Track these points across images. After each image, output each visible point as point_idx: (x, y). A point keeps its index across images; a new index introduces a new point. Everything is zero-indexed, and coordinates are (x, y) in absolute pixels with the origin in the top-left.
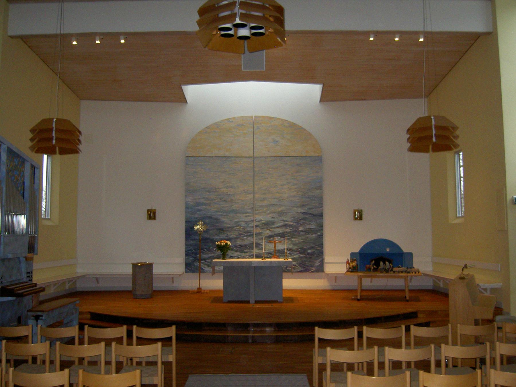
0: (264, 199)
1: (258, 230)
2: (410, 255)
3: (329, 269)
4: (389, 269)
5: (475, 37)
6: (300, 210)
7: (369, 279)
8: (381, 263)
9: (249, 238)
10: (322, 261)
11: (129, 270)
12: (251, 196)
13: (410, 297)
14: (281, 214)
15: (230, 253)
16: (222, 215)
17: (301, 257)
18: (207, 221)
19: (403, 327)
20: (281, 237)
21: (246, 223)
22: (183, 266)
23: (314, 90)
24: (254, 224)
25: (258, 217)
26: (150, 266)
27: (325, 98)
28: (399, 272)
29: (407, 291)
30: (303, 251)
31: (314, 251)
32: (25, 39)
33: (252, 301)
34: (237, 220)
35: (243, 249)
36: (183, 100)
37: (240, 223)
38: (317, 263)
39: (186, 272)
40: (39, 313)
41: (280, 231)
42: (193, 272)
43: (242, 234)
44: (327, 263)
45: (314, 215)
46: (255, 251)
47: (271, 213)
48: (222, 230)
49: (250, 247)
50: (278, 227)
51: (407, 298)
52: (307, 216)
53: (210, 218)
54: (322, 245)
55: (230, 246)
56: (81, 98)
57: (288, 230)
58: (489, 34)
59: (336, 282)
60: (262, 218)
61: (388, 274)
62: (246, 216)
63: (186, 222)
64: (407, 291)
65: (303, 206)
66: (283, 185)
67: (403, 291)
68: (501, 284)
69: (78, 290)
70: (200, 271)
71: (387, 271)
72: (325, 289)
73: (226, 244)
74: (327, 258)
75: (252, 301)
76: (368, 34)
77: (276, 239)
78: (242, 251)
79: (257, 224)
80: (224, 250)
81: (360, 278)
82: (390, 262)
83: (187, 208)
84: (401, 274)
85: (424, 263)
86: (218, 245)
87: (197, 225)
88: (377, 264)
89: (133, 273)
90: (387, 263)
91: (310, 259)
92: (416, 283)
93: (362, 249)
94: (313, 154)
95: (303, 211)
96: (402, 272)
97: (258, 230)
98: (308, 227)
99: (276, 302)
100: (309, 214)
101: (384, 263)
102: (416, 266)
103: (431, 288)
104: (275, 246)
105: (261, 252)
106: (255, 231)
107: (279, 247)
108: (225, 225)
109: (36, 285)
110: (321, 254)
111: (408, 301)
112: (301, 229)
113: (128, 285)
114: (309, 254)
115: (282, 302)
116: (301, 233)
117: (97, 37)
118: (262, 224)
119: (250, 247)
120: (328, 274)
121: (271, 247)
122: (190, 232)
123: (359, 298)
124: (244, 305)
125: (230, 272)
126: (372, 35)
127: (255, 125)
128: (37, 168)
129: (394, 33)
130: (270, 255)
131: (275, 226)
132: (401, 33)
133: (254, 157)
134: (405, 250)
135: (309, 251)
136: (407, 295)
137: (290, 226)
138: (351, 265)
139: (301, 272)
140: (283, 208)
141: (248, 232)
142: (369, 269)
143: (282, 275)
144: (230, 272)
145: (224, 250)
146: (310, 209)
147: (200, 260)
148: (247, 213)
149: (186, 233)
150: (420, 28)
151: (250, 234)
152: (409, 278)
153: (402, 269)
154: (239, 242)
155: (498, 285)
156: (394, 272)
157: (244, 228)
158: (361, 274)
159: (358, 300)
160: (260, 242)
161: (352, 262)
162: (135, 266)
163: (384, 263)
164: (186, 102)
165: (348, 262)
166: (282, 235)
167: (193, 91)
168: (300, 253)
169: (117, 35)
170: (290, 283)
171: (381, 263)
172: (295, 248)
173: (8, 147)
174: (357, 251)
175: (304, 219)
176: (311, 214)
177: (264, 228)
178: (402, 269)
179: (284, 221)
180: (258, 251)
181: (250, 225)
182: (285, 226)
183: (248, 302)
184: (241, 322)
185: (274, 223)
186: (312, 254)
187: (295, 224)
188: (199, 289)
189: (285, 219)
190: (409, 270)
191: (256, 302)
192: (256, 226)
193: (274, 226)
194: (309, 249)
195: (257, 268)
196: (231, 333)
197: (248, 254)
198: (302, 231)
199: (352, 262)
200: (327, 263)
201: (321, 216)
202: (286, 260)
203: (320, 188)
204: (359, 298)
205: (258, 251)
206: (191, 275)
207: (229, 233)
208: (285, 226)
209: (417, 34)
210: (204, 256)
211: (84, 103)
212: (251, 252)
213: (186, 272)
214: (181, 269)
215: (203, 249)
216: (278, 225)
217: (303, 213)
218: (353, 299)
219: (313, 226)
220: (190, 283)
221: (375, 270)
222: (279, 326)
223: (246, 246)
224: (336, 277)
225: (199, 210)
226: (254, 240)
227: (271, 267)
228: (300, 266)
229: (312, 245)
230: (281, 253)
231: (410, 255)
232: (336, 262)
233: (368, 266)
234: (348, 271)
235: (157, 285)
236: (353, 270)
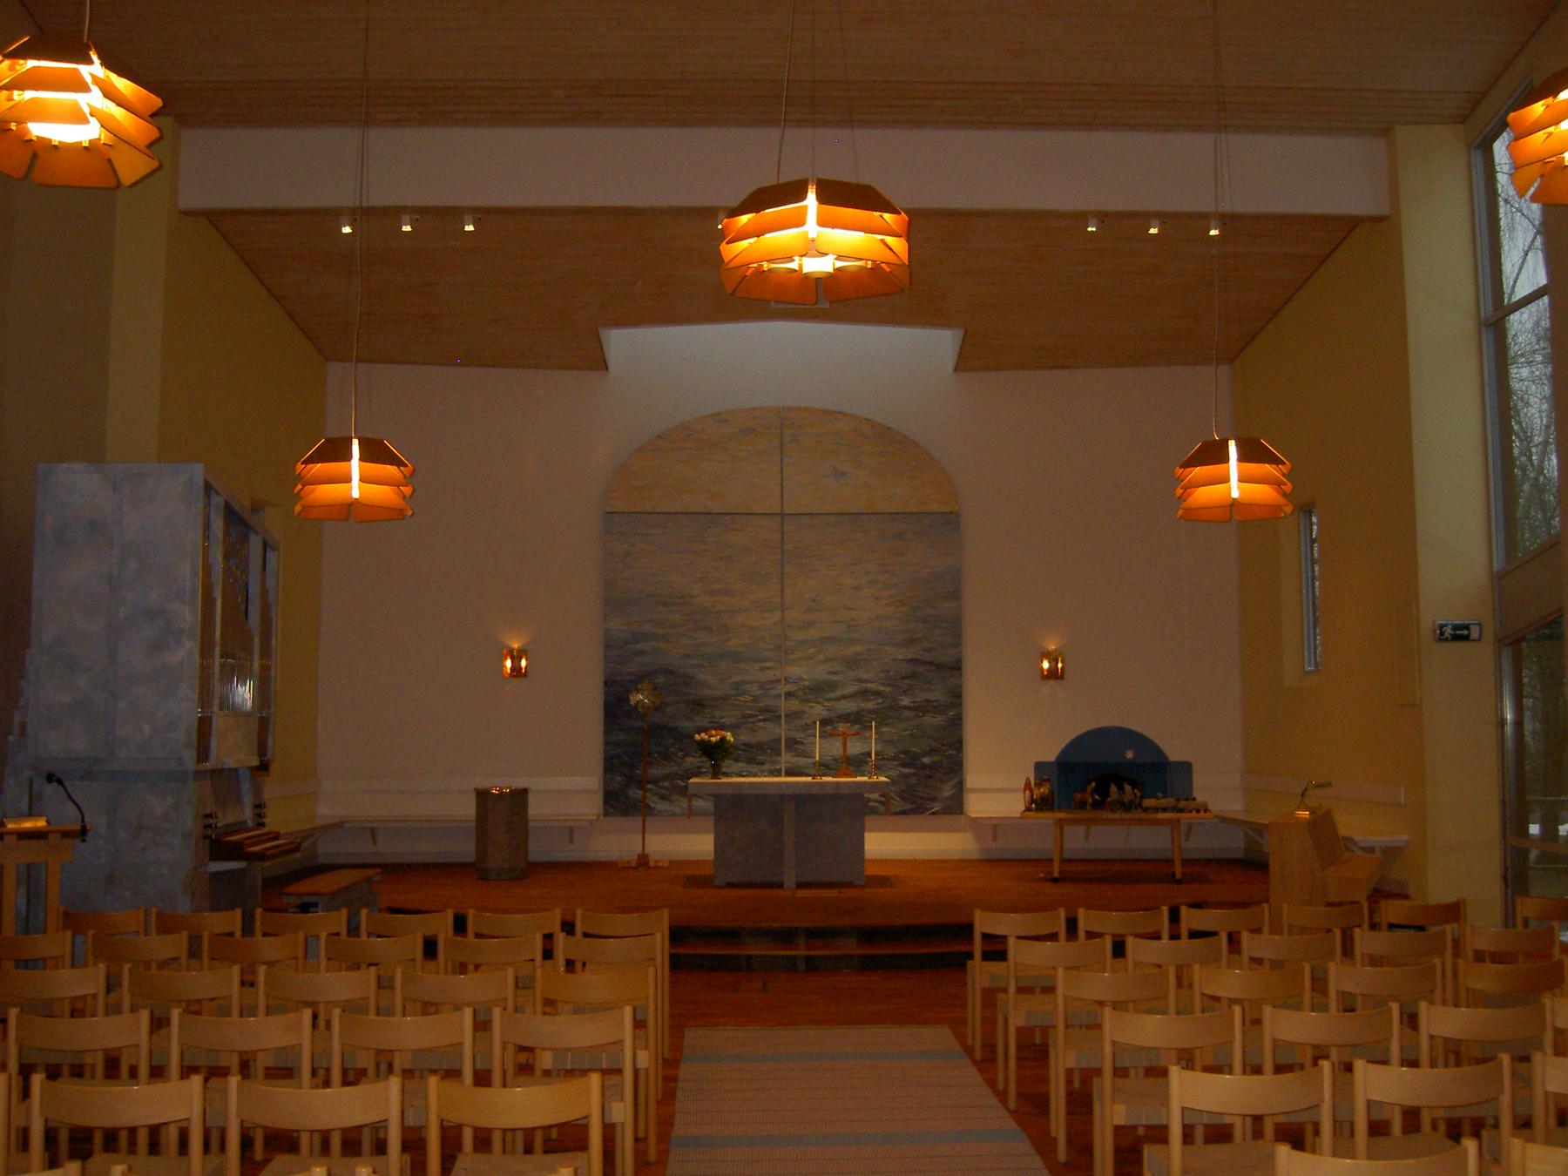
0: (810, 624)
1: (794, 705)
2: (1186, 767)
3: (978, 806)
4: (1131, 802)
5: (1343, 229)
6: (902, 654)
7: (1080, 830)
8: (1113, 789)
9: (769, 725)
10: (960, 786)
11: (467, 809)
12: (777, 616)
13: (1183, 874)
14: (852, 662)
15: (728, 764)
16: (700, 666)
17: (907, 776)
18: (661, 680)
19: (1165, 909)
20: (854, 722)
21: (762, 686)
22: (598, 799)
23: (941, 343)
24: (783, 689)
25: (794, 671)
26: (520, 795)
27: (963, 363)
28: (1157, 810)
29: (1178, 864)
30: (910, 759)
31: (936, 758)
32: (214, 217)
33: (790, 880)
34: (739, 678)
35: (755, 754)
36: (599, 363)
37: (747, 687)
38: (947, 791)
39: (606, 814)
40: (310, 899)
41: (848, 706)
42: (626, 812)
43: (751, 716)
44: (975, 790)
45: (940, 667)
46: (786, 759)
47: (827, 660)
48: (698, 705)
49: (773, 748)
50: (844, 697)
51: (1178, 876)
52: (921, 669)
53: (667, 672)
54: (958, 745)
55: (732, 746)
56: (327, 360)
57: (870, 705)
58: (1380, 219)
59: (994, 838)
60: (803, 671)
61: (1130, 816)
62: (762, 669)
63: (605, 683)
64: (1178, 864)
65: (910, 642)
66: (857, 588)
67: (1169, 862)
68: (1405, 837)
69: (321, 860)
70: (641, 810)
71: (1127, 807)
72: (966, 857)
73: (723, 739)
74: (972, 779)
75: (790, 880)
76: (1082, 217)
77: (841, 727)
78: (751, 761)
79: (790, 688)
80: (715, 754)
81: (1061, 824)
82: (1134, 785)
83: (608, 647)
84: (1161, 816)
85: (1220, 789)
86: (702, 741)
87: (638, 691)
88: (1105, 793)
89: (478, 815)
90: (1128, 788)
91: (930, 782)
92: (1200, 844)
93: (1065, 752)
94: (935, 507)
95: (910, 656)
96: (1164, 810)
97: (794, 705)
98: (924, 696)
99: (850, 885)
100: (925, 663)
101: (1121, 789)
102: (1200, 795)
103: (1240, 855)
104: (845, 745)
105: (802, 761)
106: (784, 706)
107: (855, 748)
108: (708, 692)
109: (277, 836)
110: (955, 767)
111: (1178, 882)
112: (906, 701)
113: (466, 850)
114: (924, 767)
115: (863, 887)
116: (907, 713)
117: (406, 218)
118: (805, 687)
119: (773, 748)
120: (975, 820)
121: (835, 748)
122: (616, 708)
123: (1056, 874)
124: (770, 892)
125: (733, 811)
126: (1091, 221)
127: (782, 429)
128: (273, 549)
129: (1147, 217)
130: (826, 767)
131: (839, 693)
132: (1163, 217)
133: (782, 515)
134: (1174, 755)
135: (926, 760)
136: (1178, 870)
137: (878, 693)
138: (1036, 793)
139: (904, 813)
140: (859, 648)
141: (765, 710)
142: (1082, 805)
143: (863, 823)
144: (733, 811)
145: (715, 754)
146: (929, 650)
147: (641, 783)
148: (764, 660)
149: (606, 712)
150: (1206, 206)
151: (771, 714)
152: (1183, 829)
153: (1163, 802)
154: (745, 737)
155: (1401, 838)
156: (1146, 810)
157: (756, 699)
158: (1062, 815)
159: (1055, 880)
160: (798, 735)
161: (1038, 785)
162: (482, 795)
163: (1121, 789)
164: (605, 367)
165: (1027, 786)
166: (857, 719)
167: (620, 342)
168: (904, 765)
169: (455, 214)
170: (885, 844)
171: (1113, 789)
172: (890, 752)
173: (227, 506)
174: (1051, 756)
175: (913, 675)
176: (930, 663)
177: (809, 701)
178: (1163, 802)
179: (860, 681)
180: (794, 760)
181: (774, 692)
182: (865, 694)
183: (781, 886)
184: (776, 925)
185: (832, 686)
186: (934, 767)
187: (889, 689)
188: (643, 860)
189: (865, 676)
190: (1182, 804)
191: (800, 886)
192: (789, 695)
193: (833, 695)
194: (925, 754)
195: (802, 799)
196: (758, 950)
197: (767, 767)
198: (908, 708)
199: (1038, 785)
200: (975, 790)
201: (957, 667)
202: (875, 779)
203: (956, 595)
204: (1056, 874)
205: (794, 760)
206: (619, 821)
207: (718, 713)
208: (865, 694)
209: (1204, 219)
210: (655, 772)
211: (335, 370)
212: (776, 762)
213: (606, 814)
214: (592, 806)
215: (649, 755)
216: (846, 691)
217: (910, 661)
218: (1045, 880)
219: (936, 695)
220: (618, 842)
221: (1097, 805)
222: (869, 935)
223: (761, 747)
224: (996, 827)
225: (643, 653)
226: (782, 730)
227: (835, 797)
228: (903, 799)
229: (934, 745)
230: (856, 764)
231: (1186, 767)
232: (996, 787)
233: (1079, 795)
234: (1028, 809)
235: (538, 850)
236: (1041, 804)
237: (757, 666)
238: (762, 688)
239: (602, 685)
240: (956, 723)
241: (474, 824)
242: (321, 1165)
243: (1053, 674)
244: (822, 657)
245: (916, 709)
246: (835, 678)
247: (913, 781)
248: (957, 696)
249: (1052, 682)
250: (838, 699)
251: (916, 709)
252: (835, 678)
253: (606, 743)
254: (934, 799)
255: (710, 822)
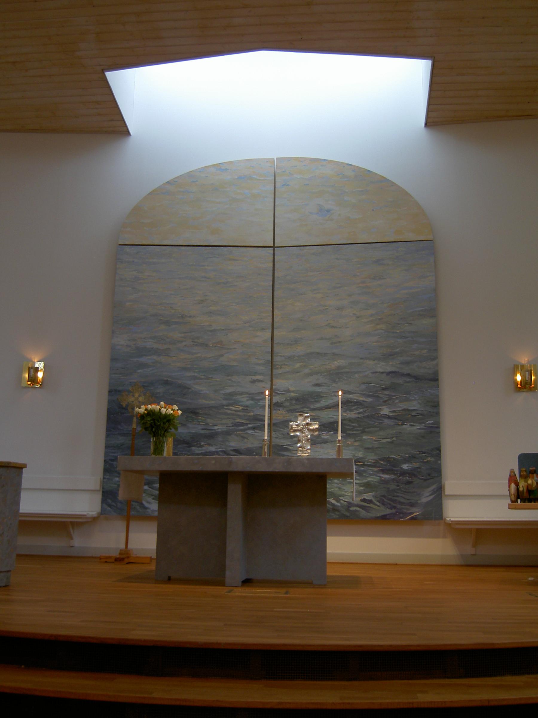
0: (296, 342)
3: (456, 511)
6: (382, 367)
10: (440, 490)
14: (336, 375)
16: (195, 378)
30: (389, 466)
34: (230, 390)
38: (426, 497)
43: (242, 424)
47: (310, 374)
52: (400, 381)
54: (437, 452)
62: (254, 382)
74: (450, 485)
95: (389, 369)
98: (404, 405)
100: (403, 375)
110: (433, 474)
112: (386, 411)
114: (404, 473)
116: (387, 421)
118: (291, 399)
135: (405, 467)
137: (358, 404)
139: (384, 518)
146: (407, 363)
148: (256, 374)
157: (246, 409)
164: (127, 133)
168: (383, 471)
172: (371, 458)
175: (393, 387)
176: (408, 375)
177: (295, 411)
185: (318, 397)
186: (412, 473)
187: (370, 400)
193: (317, 405)
198: (389, 417)
203: (432, 312)
207: (209, 421)
217: (389, 373)
219: (415, 405)
229: (414, 452)
237: (249, 378)
238: (252, 399)
239: (107, 393)
240: (435, 431)
241: (328, 533)
242: (301, 460)
243: (526, 385)
244: (307, 371)
245: (395, 418)
246: (318, 389)
247: (393, 486)
248: (435, 405)
249: (524, 395)
250: (321, 409)
251: (395, 418)
252: (318, 389)
253: (107, 447)
254: (412, 505)
255: (329, 559)
